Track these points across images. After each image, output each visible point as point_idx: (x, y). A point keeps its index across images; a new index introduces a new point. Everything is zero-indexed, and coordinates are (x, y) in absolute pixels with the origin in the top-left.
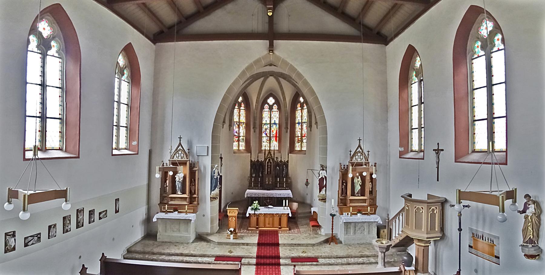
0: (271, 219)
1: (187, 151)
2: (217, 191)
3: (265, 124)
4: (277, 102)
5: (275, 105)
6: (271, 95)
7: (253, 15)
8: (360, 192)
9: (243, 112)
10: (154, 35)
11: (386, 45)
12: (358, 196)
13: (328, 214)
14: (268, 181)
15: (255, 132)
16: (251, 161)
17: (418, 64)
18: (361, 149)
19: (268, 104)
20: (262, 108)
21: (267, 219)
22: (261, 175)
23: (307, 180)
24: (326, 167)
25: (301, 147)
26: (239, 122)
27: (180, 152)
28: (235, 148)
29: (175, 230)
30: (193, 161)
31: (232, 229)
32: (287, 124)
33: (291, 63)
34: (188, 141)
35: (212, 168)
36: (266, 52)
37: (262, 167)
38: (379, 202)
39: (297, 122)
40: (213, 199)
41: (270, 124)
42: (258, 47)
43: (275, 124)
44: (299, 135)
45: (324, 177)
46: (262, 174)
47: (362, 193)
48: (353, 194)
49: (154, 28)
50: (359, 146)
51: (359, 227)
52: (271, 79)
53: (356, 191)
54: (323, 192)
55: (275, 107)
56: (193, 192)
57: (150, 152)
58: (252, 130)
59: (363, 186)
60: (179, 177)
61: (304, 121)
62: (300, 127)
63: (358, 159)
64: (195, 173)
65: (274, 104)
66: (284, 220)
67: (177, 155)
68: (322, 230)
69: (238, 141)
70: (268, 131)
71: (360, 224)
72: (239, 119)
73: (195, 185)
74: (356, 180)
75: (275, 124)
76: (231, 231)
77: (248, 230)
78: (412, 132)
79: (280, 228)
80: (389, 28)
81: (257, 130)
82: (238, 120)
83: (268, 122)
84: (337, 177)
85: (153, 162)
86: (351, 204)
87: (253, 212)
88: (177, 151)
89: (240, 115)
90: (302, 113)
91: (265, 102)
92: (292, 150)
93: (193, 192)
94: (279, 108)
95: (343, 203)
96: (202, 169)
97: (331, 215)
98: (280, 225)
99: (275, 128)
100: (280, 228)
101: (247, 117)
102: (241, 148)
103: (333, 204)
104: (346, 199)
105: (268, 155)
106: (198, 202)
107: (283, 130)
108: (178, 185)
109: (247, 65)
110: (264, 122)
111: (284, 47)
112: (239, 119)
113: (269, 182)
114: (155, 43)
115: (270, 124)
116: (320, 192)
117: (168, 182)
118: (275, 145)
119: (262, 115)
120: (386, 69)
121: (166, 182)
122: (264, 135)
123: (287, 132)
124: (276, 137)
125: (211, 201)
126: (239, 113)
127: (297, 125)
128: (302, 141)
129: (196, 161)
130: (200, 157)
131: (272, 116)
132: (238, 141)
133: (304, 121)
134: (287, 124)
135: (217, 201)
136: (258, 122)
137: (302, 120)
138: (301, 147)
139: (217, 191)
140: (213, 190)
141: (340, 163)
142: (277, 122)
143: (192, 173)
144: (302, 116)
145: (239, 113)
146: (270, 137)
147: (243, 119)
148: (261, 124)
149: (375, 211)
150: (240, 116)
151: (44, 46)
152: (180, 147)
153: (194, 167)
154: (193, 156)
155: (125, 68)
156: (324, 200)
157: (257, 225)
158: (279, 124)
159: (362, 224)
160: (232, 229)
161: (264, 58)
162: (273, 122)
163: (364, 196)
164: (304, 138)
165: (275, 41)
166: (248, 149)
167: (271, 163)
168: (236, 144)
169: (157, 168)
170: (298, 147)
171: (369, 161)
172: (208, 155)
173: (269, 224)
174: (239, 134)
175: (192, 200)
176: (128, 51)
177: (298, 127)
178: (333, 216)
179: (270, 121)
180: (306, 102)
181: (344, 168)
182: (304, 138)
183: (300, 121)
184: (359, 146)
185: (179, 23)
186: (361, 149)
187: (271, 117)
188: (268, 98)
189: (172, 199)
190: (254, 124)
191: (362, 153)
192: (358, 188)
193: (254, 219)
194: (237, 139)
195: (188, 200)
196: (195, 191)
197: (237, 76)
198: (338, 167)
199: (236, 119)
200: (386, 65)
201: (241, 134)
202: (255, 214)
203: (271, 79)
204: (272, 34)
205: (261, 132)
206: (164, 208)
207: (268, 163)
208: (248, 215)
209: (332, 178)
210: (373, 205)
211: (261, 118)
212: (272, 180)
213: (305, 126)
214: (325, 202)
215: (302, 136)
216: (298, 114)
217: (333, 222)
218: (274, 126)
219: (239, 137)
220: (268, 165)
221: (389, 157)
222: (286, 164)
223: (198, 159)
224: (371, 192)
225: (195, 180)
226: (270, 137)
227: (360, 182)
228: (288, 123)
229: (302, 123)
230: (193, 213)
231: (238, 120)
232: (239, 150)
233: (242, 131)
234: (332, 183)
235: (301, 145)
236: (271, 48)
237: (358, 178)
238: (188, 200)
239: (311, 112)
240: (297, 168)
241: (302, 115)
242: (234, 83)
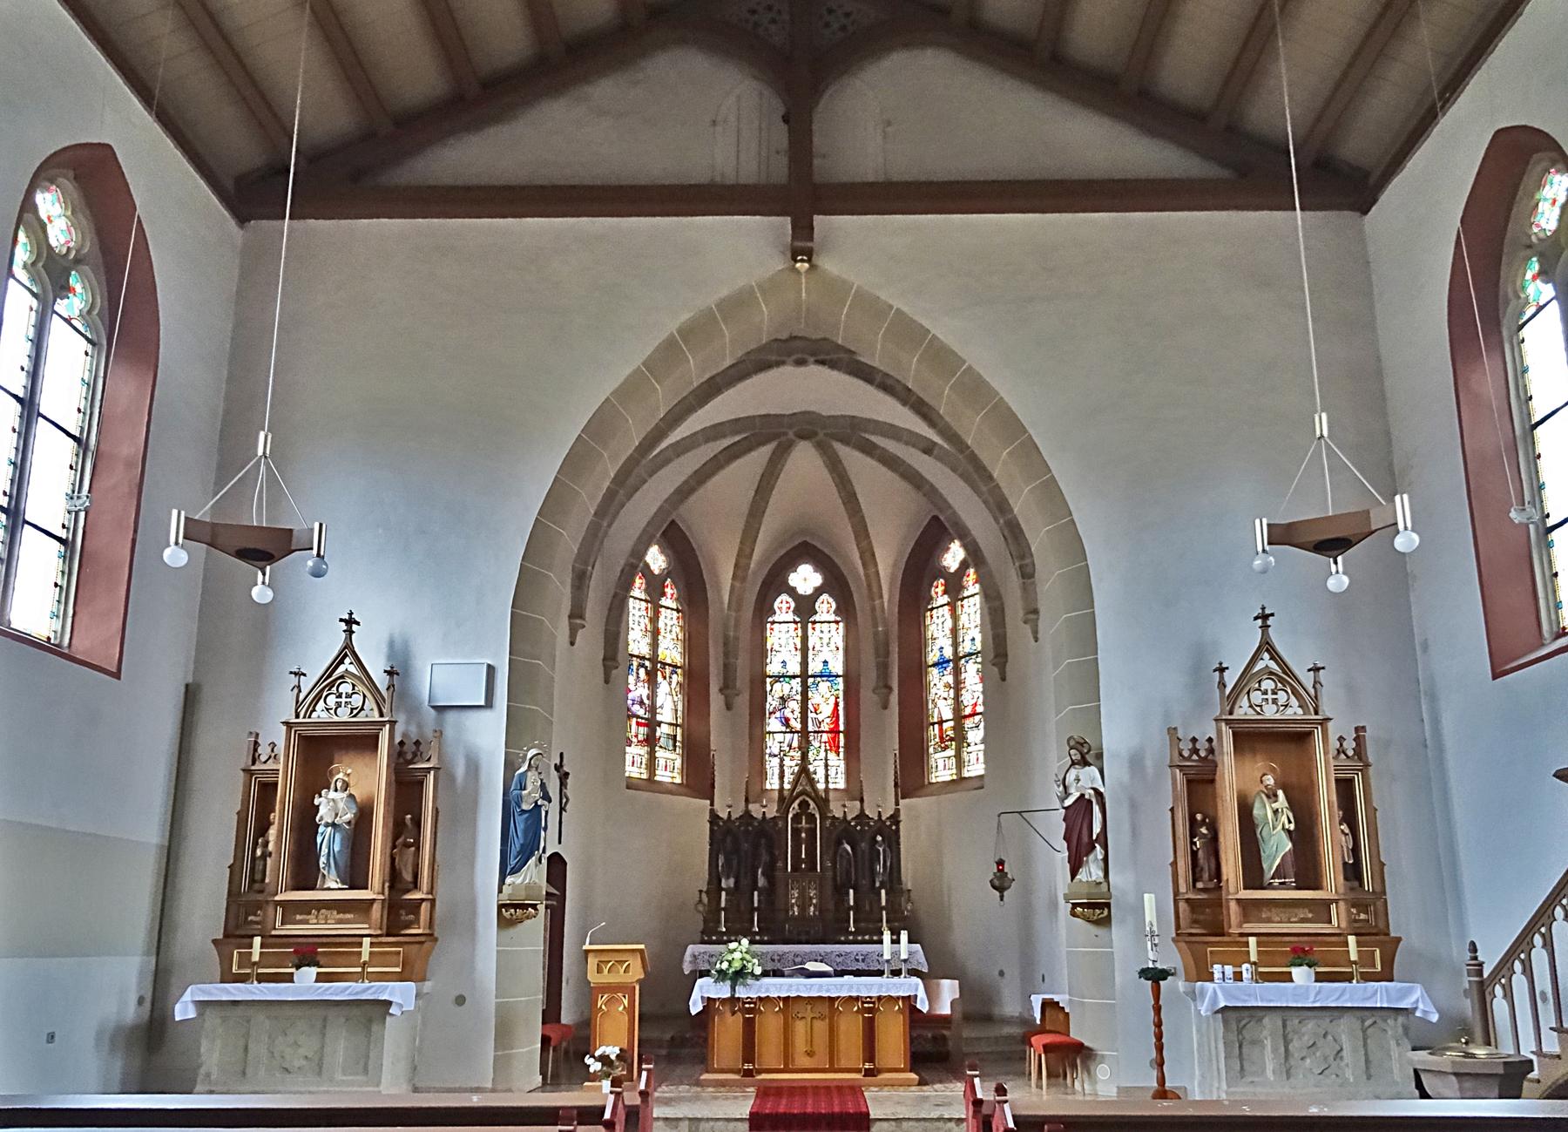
0: (821, 1027)
1: (381, 680)
2: (534, 874)
3: (778, 678)
4: (835, 583)
5: (825, 597)
6: (805, 551)
7: (714, 123)
8: (1290, 870)
9: (670, 621)
10: (240, 180)
11: (1365, 211)
12: (1283, 886)
13: (1125, 975)
14: (800, 900)
15: (729, 707)
16: (714, 818)
17: (1547, 219)
18: (1275, 656)
19: (792, 592)
20: (764, 610)
21: (800, 1028)
22: (761, 882)
23: (1000, 863)
24: (1100, 756)
25: (960, 764)
26: (654, 659)
27: (345, 688)
28: (635, 771)
29: (297, 1064)
30: (413, 729)
31: (612, 1051)
32: (883, 669)
33: (896, 304)
34: (391, 644)
35: (510, 766)
36: (778, 264)
37: (770, 849)
38: (1403, 918)
39: (933, 657)
40: (511, 913)
41: (804, 675)
42: (742, 247)
43: (827, 676)
44: (947, 714)
45: (1089, 794)
46: (769, 875)
47: (1305, 867)
48: (1253, 876)
49: (241, 147)
50: (1266, 646)
51: (1307, 1040)
52: (804, 461)
53: (1271, 865)
54: (1092, 871)
55: (826, 607)
56: (408, 877)
57: (191, 697)
58: (716, 700)
59: (1304, 835)
60: (332, 806)
61: (966, 647)
62: (950, 679)
63: (1270, 705)
64: (421, 784)
65: (818, 592)
66: (893, 1038)
67: (332, 700)
68: (1102, 1071)
69: (651, 741)
70: (794, 705)
71: (1310, 1025)
72: (655, 645)
73: (417, 845)
74: (1263, 811)
75: (827, 676)
76: (604, 1059)
77: (698, 1083)
78: (1549, 545)
79: (869, 1073)
80: (1359, 144)
81: (743, 701)
82: (645, 650)
83: (794, 668)
84: (1168, 791)
85: (207, 739)
86: (1248, 927)
87: (723, 991)
88: (330, 680)
89: (655, 630)
90: (955, 617)
91: (775, 582)
92: (912, 778)
93: (408, 877)
94: (845, 610)
95: (1204, 924)
96: (460, 771)
97: (1145, 973)
98: (870, 1055)
99: (825, 699)
100: (869, 1073)
101: (693, 643)
102: (662, 776)
103: (1150, 915)
104: (1218, 904)
105: (795, 783)
106: (431, 924)
107: (868, 697)
108: (329, 843)
109: (685, 316)
110: (773, 668)
111: (858, 247)
112: (655, 645)
113: (803, 909)
114: (242, 219)
115: (804, 675)
116: (1074, 874)
117: (273, 832)
118: (831, 771)
119: (764, 640)
120: (1371, 307)
121: (262, 829)
122: (774, 724)
123: (885, 707)
124: (835, 731)
125: (504, 923)
126: (654, 619)
127: (934, 671)
128: (960, 738)
129: (429, 734)
130: (451, 717)
131: (813, 641)
132: (651, 741)
133: (966, 647)
134: (883, 669)
135: (536, 926)
136: (742, 663)
137: (955, 645)
138: (960, 764)
139: (534, 874)
140: (515, 871)
141: (1172, 731)
142: (837, 666)
143: (406, 788)
144: (954, 631)
145: (654, 619)
146: (804, 733)
147: (671, 651)
148: (759, 682)
149: (1388, 962)
150: (655, 633)
151: (805, 608)
152: (348, 665)
153: (417, 754)
154: (413, 710)
155: (78, 261)
156: (1096, 910)
157: (746, 1061)
158: (846, 676)
159: (1325, 1023)
160: (612, 1051)
161: (770, 287)
162: (815, 667)
163: (1318, 887)
164: (968, 723)
165: (817, 219)
166: (699, 777)
167: (811, 818)
168: (636, 752)
169: (175, 523)
170: (941, 768)
171: (1326, 710)
172: (489, 704)
173: (810, 1054)
174: (653, 709)
175: (398, 913)
176: (92, 174)
177: (939, 682)
178: (1156, 976)
179: (804, 663)
180: (975, 555)
181: (1195, 751)
182: (968, 723)
183: (948, 653)
184: (1266, 646)
185: (368, 136)
186: (1275, 656)
187: (806, 648)
188: (789, 562)
189: (292, 910)
190: (724, 675)
191: (1286, 677)
192: (1277, 847)
193: (727, 1031)
194: (643, 730)
195: (376, 910)
196: (416, 876)
197: (637, 361)
198: (1158, 751)
199: (638, 643)
200: (1369, 295)
201: (665, 715)
202: (733, 1000)
203: (804, 461)
204: (802, 195)
205: (758, 713)
206: (245, 960)
207: (796, 818)
208: (696, 1007)
209: (1134, 807)
210: (1375, 932)
211: (761, 652)
212: (820, 897)
213: (971, 672)
214: (1105, 922)
215: (959, 717)
216: (938, 626)
217: (1159, 1024)
218: (824, 686)
219: (652, 724)
220: (796, 832)
221: (1433, 698)
222: (889, 830)
223: (440, 722)
224: (1353, 872)
225: (417, 823)
226: (804, 733)
227: (1286, 820)
228: (890, 671)
229: (957, 658)
230: (401, 977)
231: (645, 650)
232: (651, 780)
233: (669, 703)
234: (1135, 832)
235: (958, 756)
236: (802, 248)
237: (1273, 796)
238: (376, 910)
239: (999, 597)
240: (939, 850)
241: (955, 625)
242: (629, 391)
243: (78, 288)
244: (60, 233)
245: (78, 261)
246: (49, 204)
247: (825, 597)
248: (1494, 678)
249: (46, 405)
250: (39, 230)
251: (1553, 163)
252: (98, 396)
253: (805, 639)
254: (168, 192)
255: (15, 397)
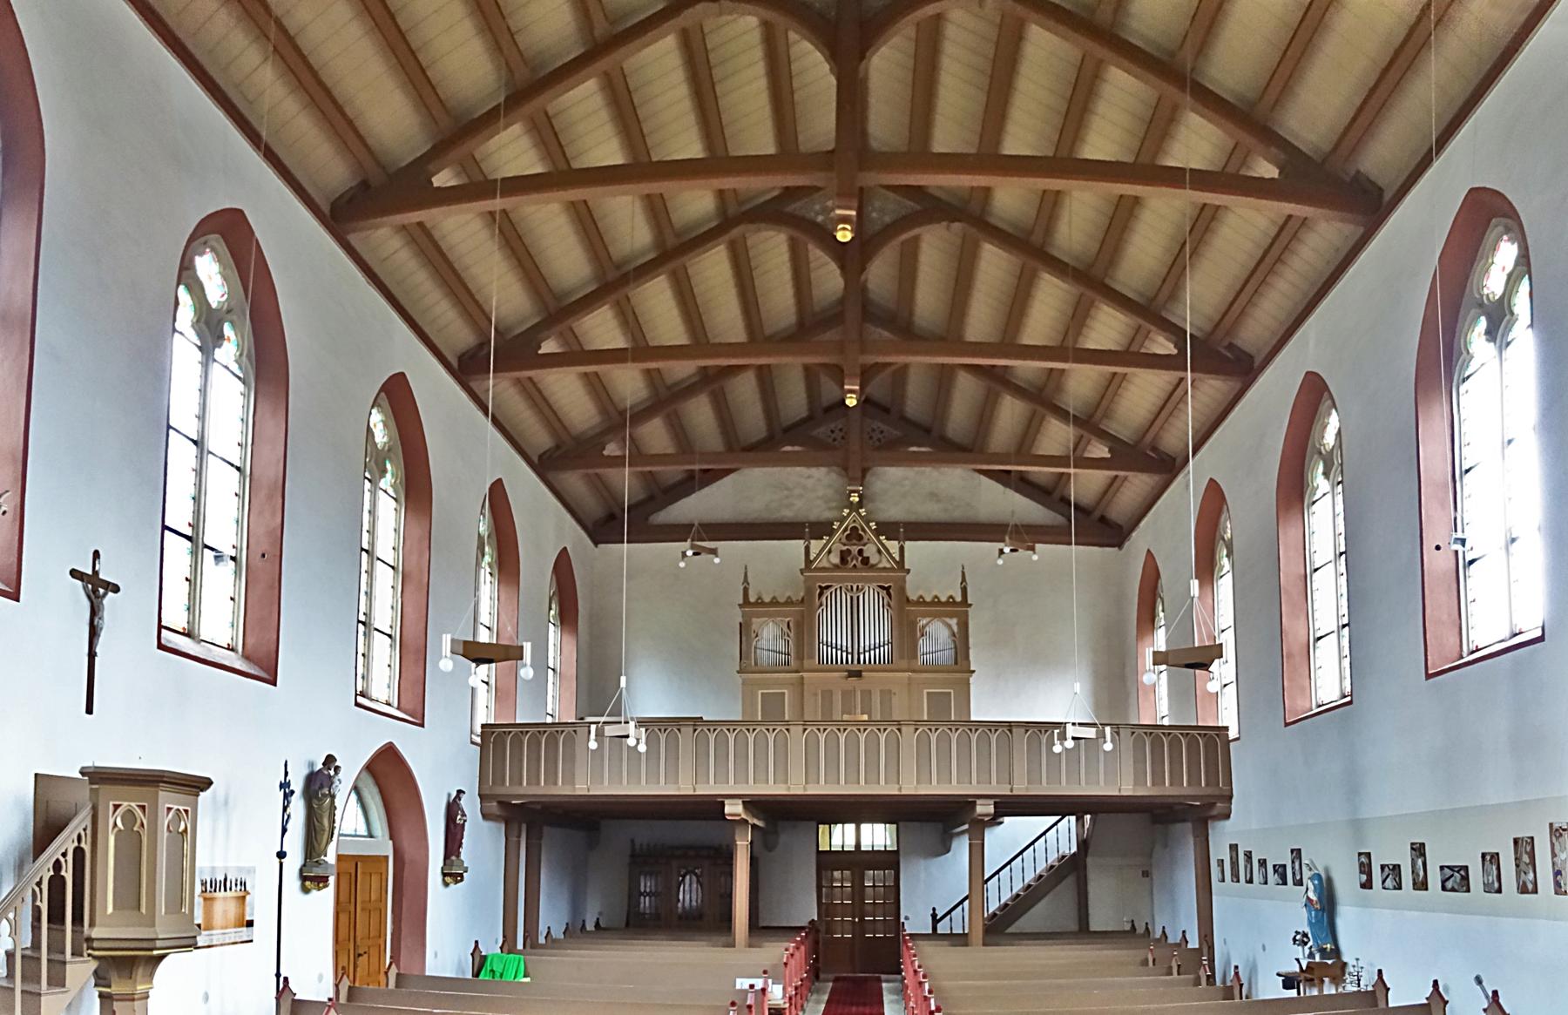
17: (1329, 439)
243: (233, 337)
244: (216, 289)
245: (229, 311)
246: (207, 267)
248: (422, 725)
249: (211, 444)
250: (197, 289)
251: (1508, 230)
252: (255, 439)
254: (290, 233)
255: (746, 591)
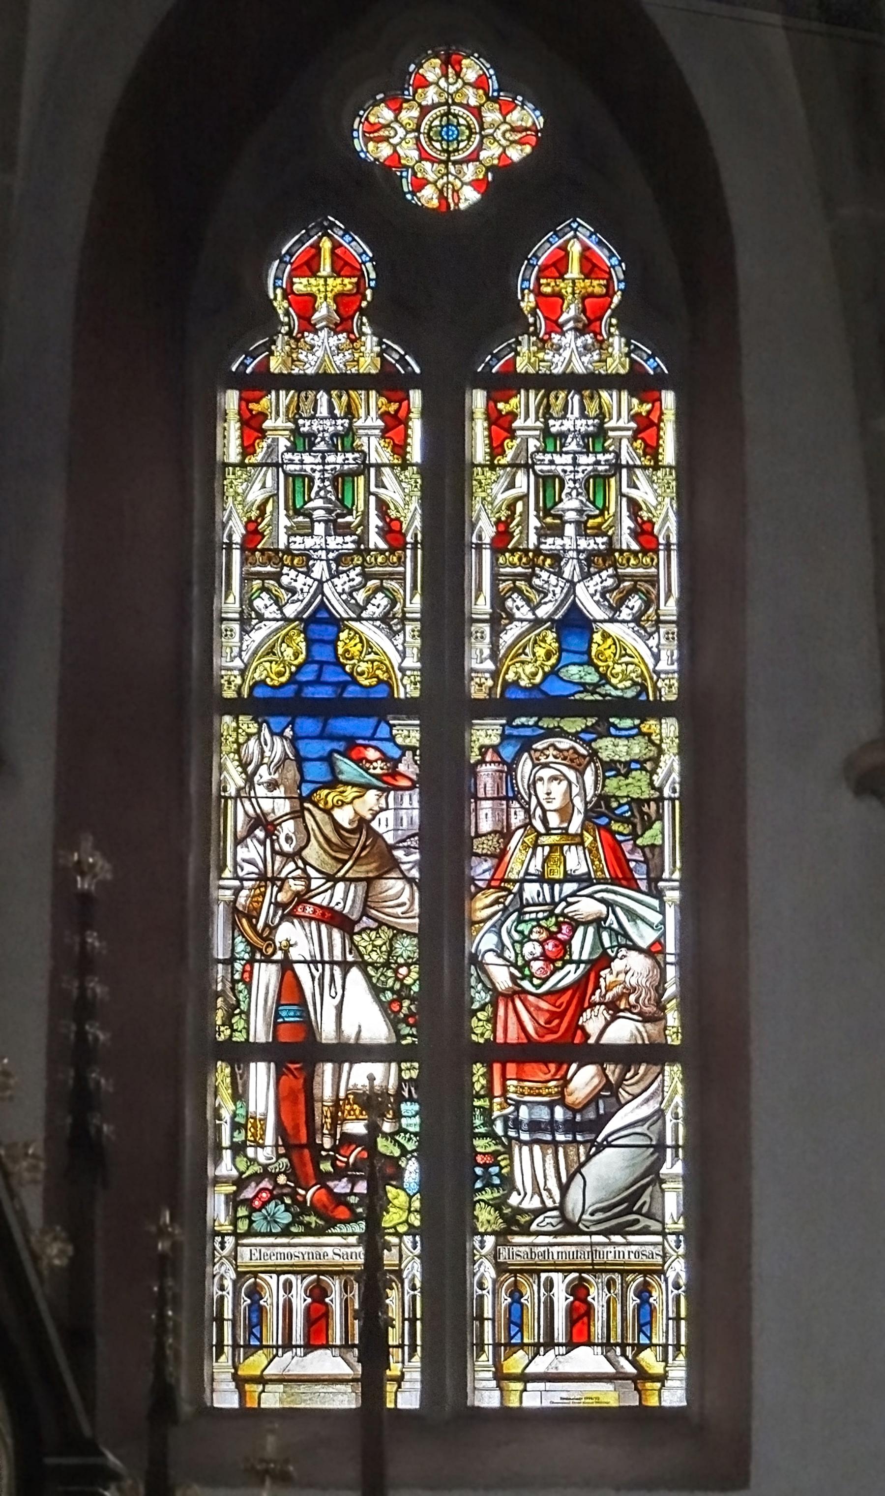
19: (371, 198)
94: (684, 313)
151: (446, 299)
247: (579, 240)
253: (446, 481)
